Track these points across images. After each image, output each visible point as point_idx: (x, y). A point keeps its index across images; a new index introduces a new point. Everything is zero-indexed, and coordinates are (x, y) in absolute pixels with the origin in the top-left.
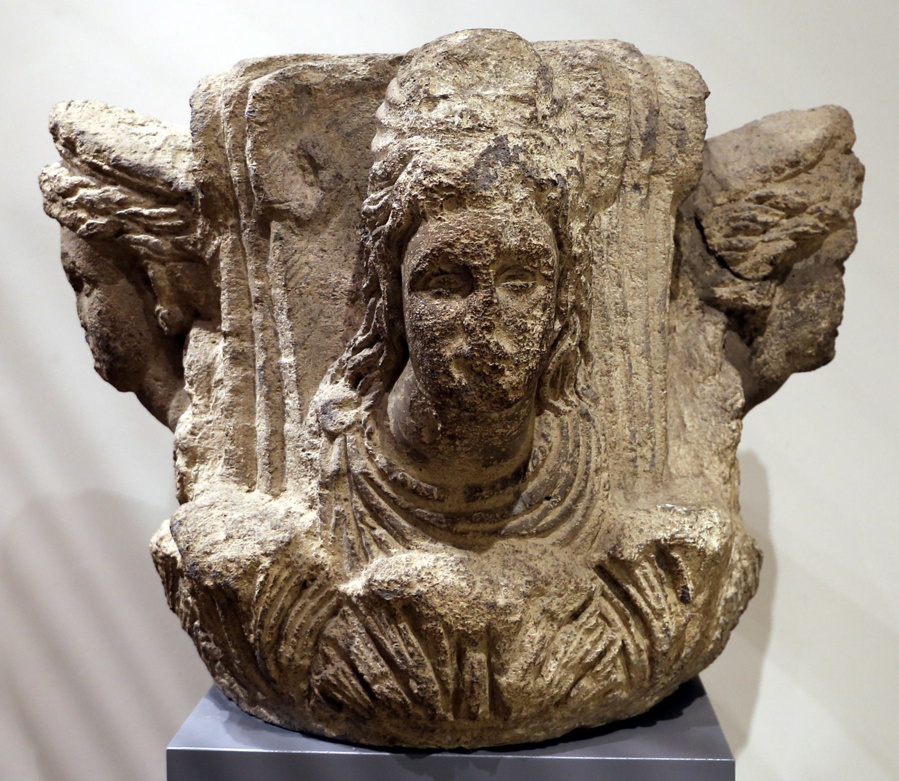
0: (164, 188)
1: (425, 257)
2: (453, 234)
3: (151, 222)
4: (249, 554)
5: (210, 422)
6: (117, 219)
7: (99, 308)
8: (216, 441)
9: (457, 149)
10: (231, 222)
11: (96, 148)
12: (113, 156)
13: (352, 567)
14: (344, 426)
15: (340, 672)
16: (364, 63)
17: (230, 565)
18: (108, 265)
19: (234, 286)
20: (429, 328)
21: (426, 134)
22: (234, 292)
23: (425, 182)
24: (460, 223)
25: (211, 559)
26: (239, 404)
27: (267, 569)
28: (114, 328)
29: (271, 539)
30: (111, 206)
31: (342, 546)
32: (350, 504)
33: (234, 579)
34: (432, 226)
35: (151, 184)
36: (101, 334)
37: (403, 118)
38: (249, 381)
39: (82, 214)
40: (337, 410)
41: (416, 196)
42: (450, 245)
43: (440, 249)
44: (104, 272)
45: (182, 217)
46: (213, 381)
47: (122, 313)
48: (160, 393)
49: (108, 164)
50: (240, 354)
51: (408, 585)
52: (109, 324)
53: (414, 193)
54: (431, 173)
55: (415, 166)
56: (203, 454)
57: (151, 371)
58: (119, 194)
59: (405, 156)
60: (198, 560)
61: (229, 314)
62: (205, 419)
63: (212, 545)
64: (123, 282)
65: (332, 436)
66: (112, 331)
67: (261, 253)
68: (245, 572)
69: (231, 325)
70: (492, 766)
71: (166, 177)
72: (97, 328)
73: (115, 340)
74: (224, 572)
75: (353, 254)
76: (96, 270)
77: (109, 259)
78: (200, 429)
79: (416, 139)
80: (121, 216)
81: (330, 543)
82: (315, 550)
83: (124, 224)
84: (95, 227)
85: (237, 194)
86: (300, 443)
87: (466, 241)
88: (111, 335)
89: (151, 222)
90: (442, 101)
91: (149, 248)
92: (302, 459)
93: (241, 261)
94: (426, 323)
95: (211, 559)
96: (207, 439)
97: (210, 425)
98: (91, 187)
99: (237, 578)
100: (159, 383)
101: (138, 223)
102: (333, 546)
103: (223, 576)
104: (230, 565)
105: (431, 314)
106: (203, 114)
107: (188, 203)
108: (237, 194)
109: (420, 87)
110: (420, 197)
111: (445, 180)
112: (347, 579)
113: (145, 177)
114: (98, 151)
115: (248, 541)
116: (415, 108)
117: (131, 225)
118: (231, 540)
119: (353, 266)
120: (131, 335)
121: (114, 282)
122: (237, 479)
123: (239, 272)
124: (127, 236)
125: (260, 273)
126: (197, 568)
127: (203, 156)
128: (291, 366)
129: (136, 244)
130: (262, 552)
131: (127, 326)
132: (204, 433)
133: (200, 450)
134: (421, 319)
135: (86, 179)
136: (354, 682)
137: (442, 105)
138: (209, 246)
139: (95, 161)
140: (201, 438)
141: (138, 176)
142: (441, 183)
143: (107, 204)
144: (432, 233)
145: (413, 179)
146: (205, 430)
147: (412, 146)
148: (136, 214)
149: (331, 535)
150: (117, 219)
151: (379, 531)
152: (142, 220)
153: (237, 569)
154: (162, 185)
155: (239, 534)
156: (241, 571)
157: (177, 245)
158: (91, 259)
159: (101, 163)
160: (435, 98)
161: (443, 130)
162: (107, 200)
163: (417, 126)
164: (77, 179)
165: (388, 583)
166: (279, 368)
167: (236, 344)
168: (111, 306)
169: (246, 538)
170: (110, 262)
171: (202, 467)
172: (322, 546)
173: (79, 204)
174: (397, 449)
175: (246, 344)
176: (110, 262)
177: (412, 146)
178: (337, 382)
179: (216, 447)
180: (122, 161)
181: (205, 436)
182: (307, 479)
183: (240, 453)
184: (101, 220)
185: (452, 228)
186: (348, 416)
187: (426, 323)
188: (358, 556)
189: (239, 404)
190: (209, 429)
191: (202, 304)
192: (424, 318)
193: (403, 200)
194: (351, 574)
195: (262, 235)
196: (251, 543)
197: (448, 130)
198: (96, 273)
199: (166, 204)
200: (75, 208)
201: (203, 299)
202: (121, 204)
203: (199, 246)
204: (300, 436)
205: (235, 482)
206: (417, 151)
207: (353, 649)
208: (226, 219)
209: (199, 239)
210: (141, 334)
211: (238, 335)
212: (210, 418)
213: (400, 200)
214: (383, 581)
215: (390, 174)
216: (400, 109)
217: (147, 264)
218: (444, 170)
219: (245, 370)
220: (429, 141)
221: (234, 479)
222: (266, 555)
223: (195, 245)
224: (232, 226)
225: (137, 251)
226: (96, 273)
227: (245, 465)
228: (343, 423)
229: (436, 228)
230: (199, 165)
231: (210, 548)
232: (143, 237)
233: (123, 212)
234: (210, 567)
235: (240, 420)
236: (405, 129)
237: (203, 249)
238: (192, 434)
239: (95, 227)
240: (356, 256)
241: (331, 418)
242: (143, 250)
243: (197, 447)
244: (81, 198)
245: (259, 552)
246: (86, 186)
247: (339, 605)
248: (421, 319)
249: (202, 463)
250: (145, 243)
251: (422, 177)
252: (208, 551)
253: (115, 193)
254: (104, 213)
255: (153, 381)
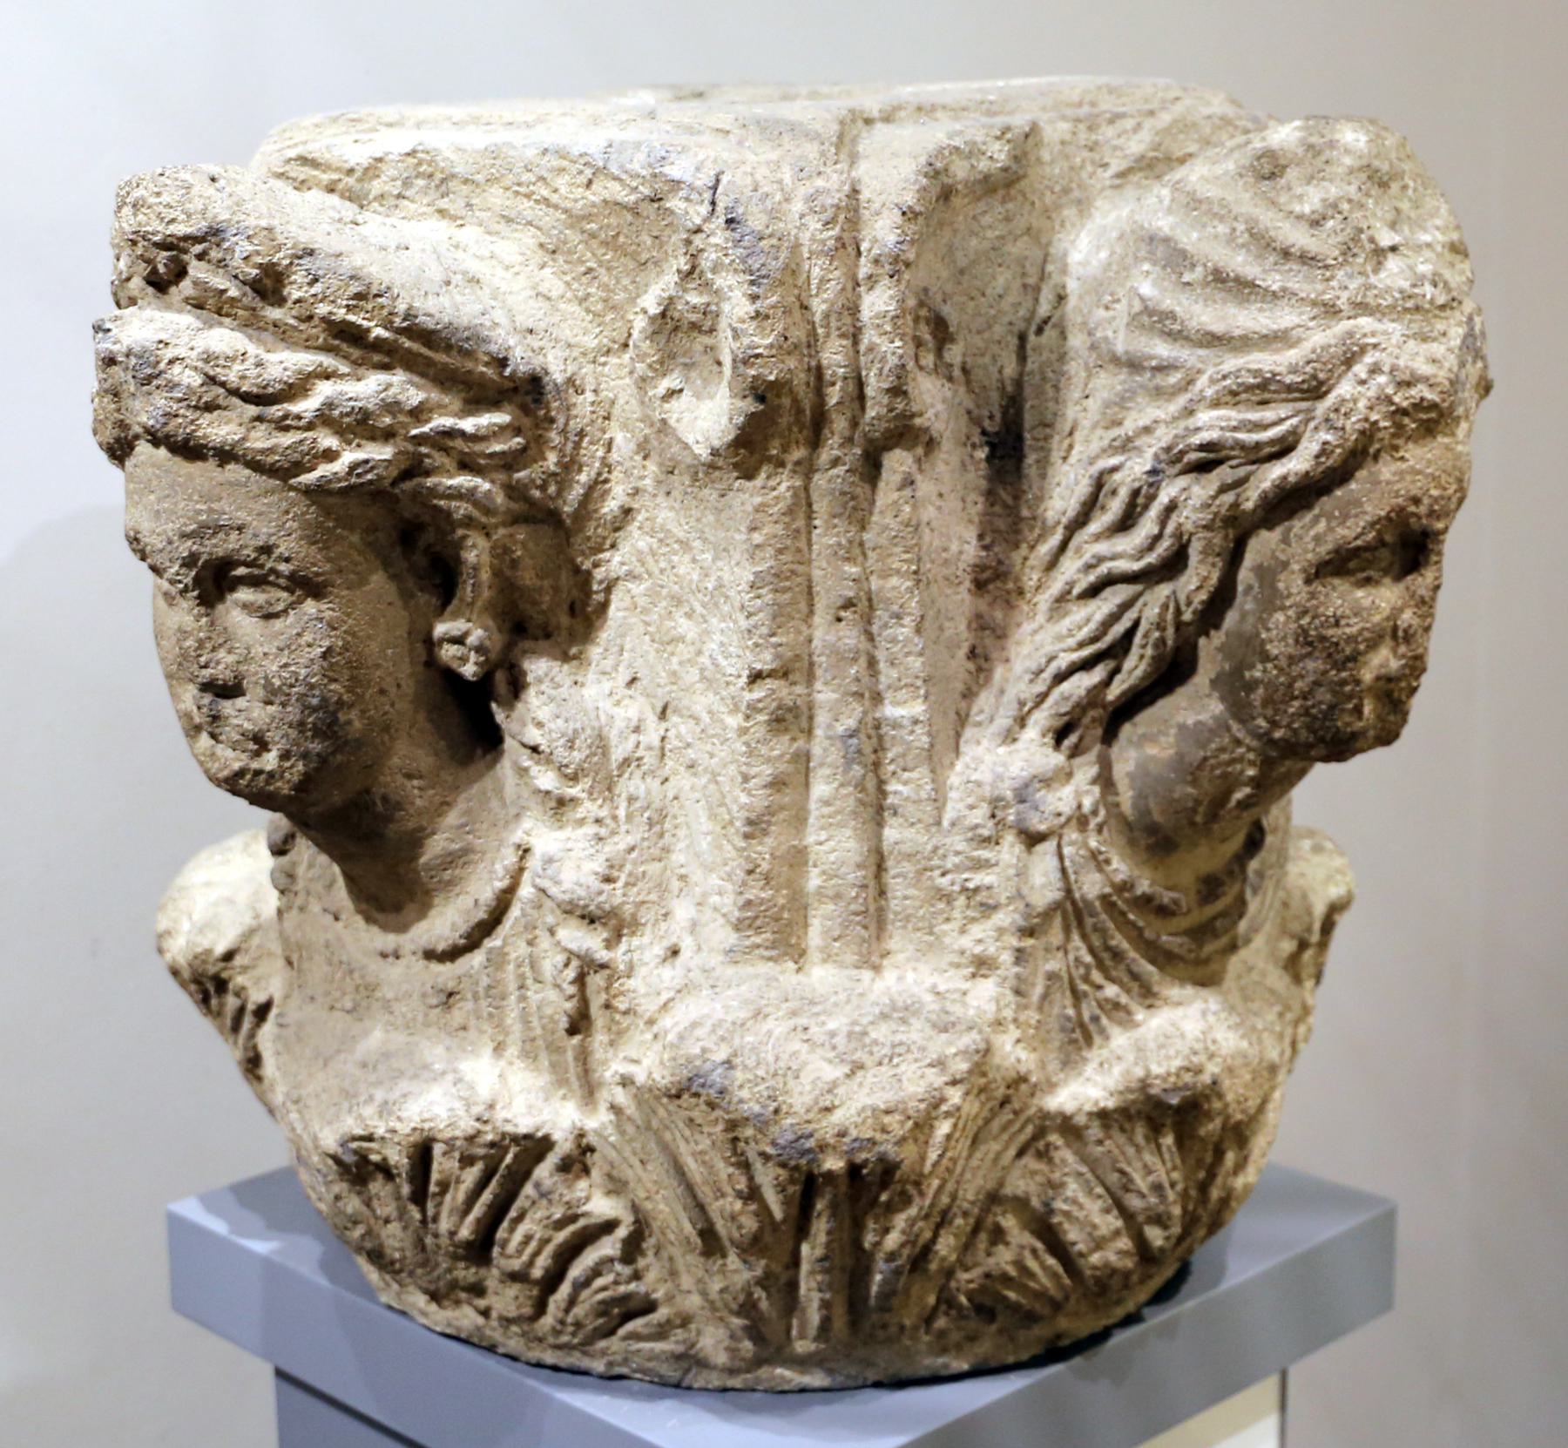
0: (490, 372)
1: (1373, 524)
2: (1421, 482)
3: (478, 447)
4: (921, 1090)
5: (632, 849)
6: (411, 448)
7: (326, 643)
8: (651, 884)
9: (1425, 339)
10: (798, 453)
11: (355, 288)
12: (401, 307)
13: (1065, 1064)
14: (1063, 819)
15: (1027, 1254)
16: (998, 138)
17: (887, 1119)
18: (352, 546)
19: (787, 579)
20: (1351, 639)
21: (1384, 315)
22: (785, 590)
23: (1396, 399)
24: (1429, 462)
25: (837, 1117)
26: (782, 808)
27: (958, 1109)
28: (355, 682)
29: (953, 1050)
30: (401, 418)
31: (1048, 1032)
32: (1063, 955)
33: (896, 1144)
34: (1386, 470)
35: (469, 365)
36: (324, 700)
37: (1334, 283)
38: (803, 761)
39: (328, 441)
40: (1043, 792)
41: (1376, 422)
42: (1416, 501)
43: (1402, 509)
44: (344, 563)
45: (518, 431)
46: (614, 765)
47: (374, 646)
48: (418, 802)
49: (388, 325)
50: (790, 710)
51: (1198, 1071)
52: (346, 674)
53: (1374, 417)
54: (1409, 384)
55: (1375, 370)
56: (634, 916)
57: (396, 761)
58: (412, 391)
59: (1354, 354)
60: (811, 1127)
61: (773, 635)
62: (622, 846)
63: (829, 1091)
64: (378, 580)
65: (1032, 839)
66: (350, 690)
67: (857, 512)
68: (916, 1125)
69: (777, 656)
70: (1169, 1330)
71: (493, 348)
72: (312, 687)
73: (351, 706)
74: (878, 1136)
75: (973, 496)
76: (329, 560)
77: (352, 529)
78: (622, 866)
79: (1365, 322)
80: (420, 440)
81: (1032, 1031)
82: (1013, 1053)
83: (427, 456)
84: (372, 468)
85: (833, 401)
86: (936, 862)
87: (1434, 492)
88: (345, 697)
89: (478, 447)
90: (1390, 255)
91: (476, 504)
92: (940, 890)
93: (803, 530)
94: (1348, 630)
95: (837, 1117)
96: (634, 885)
97: (634, 855)
98: (342, 376)
99: (901, 1141)
100: (415, 782)
101: (446, 450)
102: (1035, 1039)
103: (875, 1143)
104: (887, 1119)
105: (1356, 615)
106: (774, 241)
107: (529, 399)
108: (833, 401)
109: (1361, 231)
110: (1383, 424)
111: (1431, 396)
112: (1052, 1086)
113: (461, 350)
114: (360, 296)
115: (903, 1067)
116: (1357, 269)
117: (439, 459)
118: (860, 1073)
119: (976, 519)
120: (382, 692)
121: (363, 581)
122: (774, 953)
123: (799, 550)
124: (430, 482)
125: (856, 550)
126: (811, 1143)
127: (780, 327)
128: (916, 722)
129: (450, 497)
130: (946, 1079)
131: (378, 673)
132: (630, 874)
133: (628, 909)
134: (1337, 624)
135: (328, 361)
136: (1051, 1261)
137: (1393, 263)
138: (571, 487)
139: (351, 318)
140: (627, 884)
141: (449, 348)
142: (1422, 399)
143: (394, 417)
144: (1388, 483)
145: (1371, 393)
146: (628, 867)
147: (1365, 335)
148: (450, 433)
149: (1033, 1016)
150: (411, 448)
151: (1111, 991)
152: (458, 443)
153: (902, 1123)
154: (487, 364)
155: (877, 1057)
156: (910, 1123)
157: (514, 491)
158: (315, 535)
159: (365, 324)
160: (1383, 250)
161: (1411, 308)
162: (392, 407)
163: (1370, 300)
164: (305, 360)
165: (1178, 1075)
166: (877, 727)
167: (785, 691)
168: (354, 635)
169: (895, 1061)
170: (355, 538)
171: (636, 942)
172: (1018, 1041)
173: (324, 418)
174: (1132, 842)
175: (799, 689)
176: (355, 538)
177: (1365, 335)
178: (1015, 740)
179: (653, 897)
180: (421, 319)
181: (632, 880)
182: (955, 925)
183: (781, 901)
184: (381, 452)
185: (1419, 472)
186: (1062, 799)
187: (1348, 630)
188: (1080, 1037)
189: (782, 808)
190: (635, 863)
191: (544, 607)
192: (1343, 622)
193: (1348, 427)
194: (1062, 1076)
195: (863, 477)
196: (908, 1069)
197: (1417, 309)
198: (328, 567)
199: (494, 404)
200: (310, 427)
201: (547, 598)
202: (418, 414)
203: (552, 489)
204: (936, 849)
205: (770, 959)
206: (1375, 346)
207: (1059, 1205)
208: (785, 449)
209: (555, 474)
210: (399, 686)
211: (785, 675)
212: (630, 840)
213: (1343, 429)
214: (1169, 1074)
215: (1321, 383)
216: (1326, 267)
217: (465, 537)
218: (1427, 379)
219: (794, 739)
220: (1391, 326)
221: (767, 953)
222: (954, 1083)
223: (543, 488)
224: (798, 463)
225: (448, 514)
226: (328, 567)
227: (789, 924)
228: (1059, 815)
229: (1394, 474)
230: (771, 346)
231: (829, 1097)
232: (463, 480)
233: (426, 429)
234: (842, 1134)
235: (782, 838)
236: (1342, 303)
237: (560, 493)
238: (608, 880)
239: (372, 468)
240: (981, 499)
241: (1037, 809)
242: (461, 509)
243: (624, 903)
244: (329, 405)
245: (939, 1081)
246: (327, 376)
247: (1040, 1133)
248: (1337, 624)
249: (633, 933)
250: (469, 495)
251: (1390, 391)
252: (828, 1103)
253: (403, 387)
254: (388, 435)
255: (400, 779)
